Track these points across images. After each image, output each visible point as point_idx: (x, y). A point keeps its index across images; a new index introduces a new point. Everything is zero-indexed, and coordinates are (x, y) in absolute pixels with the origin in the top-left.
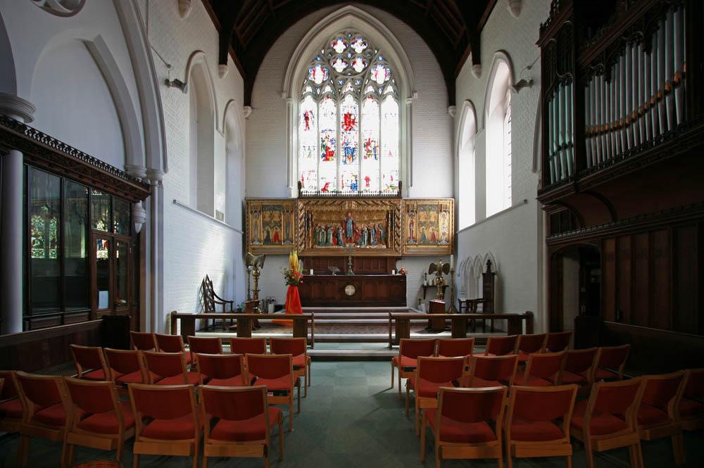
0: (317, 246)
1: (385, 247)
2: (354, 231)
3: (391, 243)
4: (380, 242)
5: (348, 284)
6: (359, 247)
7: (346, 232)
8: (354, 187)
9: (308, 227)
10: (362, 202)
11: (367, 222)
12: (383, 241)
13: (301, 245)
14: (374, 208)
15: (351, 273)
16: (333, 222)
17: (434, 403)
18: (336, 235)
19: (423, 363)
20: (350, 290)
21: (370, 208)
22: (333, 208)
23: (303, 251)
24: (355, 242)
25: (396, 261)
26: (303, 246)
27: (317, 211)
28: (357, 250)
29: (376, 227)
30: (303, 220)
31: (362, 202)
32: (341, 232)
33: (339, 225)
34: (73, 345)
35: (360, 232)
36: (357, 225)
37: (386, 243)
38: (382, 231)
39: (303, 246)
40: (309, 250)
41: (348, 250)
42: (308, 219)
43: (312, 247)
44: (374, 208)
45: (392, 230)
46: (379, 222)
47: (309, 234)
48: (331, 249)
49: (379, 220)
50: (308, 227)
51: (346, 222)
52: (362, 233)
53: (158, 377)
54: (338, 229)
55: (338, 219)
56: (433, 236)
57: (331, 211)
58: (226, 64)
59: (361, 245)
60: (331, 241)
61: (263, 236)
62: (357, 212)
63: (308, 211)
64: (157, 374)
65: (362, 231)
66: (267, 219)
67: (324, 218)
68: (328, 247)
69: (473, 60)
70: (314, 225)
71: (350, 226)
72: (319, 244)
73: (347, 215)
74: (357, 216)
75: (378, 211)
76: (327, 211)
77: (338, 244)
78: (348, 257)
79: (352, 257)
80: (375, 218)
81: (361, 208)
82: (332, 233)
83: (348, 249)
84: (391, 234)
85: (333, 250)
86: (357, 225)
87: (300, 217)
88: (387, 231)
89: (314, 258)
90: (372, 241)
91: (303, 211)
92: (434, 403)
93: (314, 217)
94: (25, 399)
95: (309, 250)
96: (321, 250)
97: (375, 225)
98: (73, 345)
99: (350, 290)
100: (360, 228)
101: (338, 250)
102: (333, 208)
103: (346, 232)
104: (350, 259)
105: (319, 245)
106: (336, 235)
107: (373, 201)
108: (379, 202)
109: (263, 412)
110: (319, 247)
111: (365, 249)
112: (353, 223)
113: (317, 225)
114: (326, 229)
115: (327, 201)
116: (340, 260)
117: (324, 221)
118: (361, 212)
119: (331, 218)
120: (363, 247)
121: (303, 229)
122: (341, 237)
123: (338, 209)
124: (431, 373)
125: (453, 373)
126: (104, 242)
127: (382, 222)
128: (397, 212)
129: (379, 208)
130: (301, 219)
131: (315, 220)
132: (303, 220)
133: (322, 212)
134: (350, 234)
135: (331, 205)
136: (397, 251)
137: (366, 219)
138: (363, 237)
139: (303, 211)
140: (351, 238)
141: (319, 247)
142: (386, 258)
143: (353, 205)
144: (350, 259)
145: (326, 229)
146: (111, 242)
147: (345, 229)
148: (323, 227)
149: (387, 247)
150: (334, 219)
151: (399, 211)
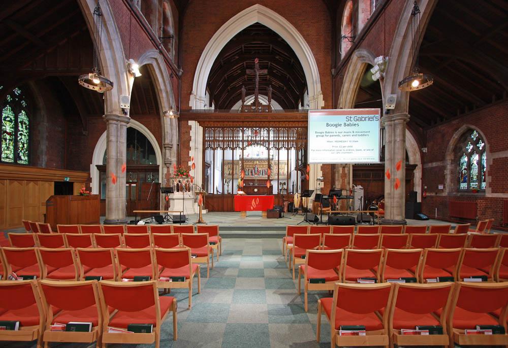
5: (254, 191)
8: (258, 155)
11: (262, 168)
15: (256, 185)
17: (304, 261)
18: (252, 172)
19: (297, 238)
20: (256, 190)
22: (251, 163)
32: (253, 171)
34: (134, 211)
48: (249, 177)
53: (88, 268)
56: (283, 173)
58: (332, 297)
61: (228, 173)
64: (87, 266)
66: (229, 167)
69: (301, 105)
71: (256, 169)
77: (252, 175)
83: (256, 177)
92: (304, 261)
96: (247, 177)
98: (134, 211)
99: (256, 190)
102: (251, 163)
106: (252, 172)
114: (248, 170)
116: (253, 181)
123: (252, 163)
124: (300, 242)
125: (314, 242)
126: (493, 219)
134: (256, 172)
145: (248, 170)
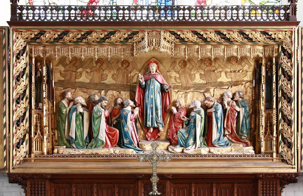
0: (63, 150)
1: (250, 150)
2: (166, 111)
3: (269, 140)
4: (236, 137)
6: (178, 149)
7: (143, 114)
9: (39, 99)
10: (189, 36)
11: (202, 88)
12: (245, 137)
13: (18, 146)
14: (220, 52)
16: (107, 88)
21: (208, 51)
22: (106, 52)
23: (25, 161)
24: (168, 139)
25: (282, 186)
26: (24, 148)
27: (62, 61)
28: (175, 158)
29: (226, 100)
30: (24, 81)
31: (189, 36)
33: (125, 95)
35: (183, 114)
36: (174, 97)
37: (254, 141)
38: (242, 111)
39: (24, 148)
40: (41, 158)
41: (149, 158)
42: (39, 81)
43: (51, 152)
44: (220, 52)
45: (269, 107)
46: (234, 89)
47: (40, 118)
49: (236, 84)
50: (39, 99)
51: (144, 89)
52: (188, 115)
54: (122, 105)
55: (120, 80)
57: (100, 61)
59: (186, 146)
60: (103, 136)
62: (173, 61)
63: (38, 59)
65: (189, 111)
67: (84, 79)
68: (95, 151)
70: (57, 93)
72: (70, 142)
73: (146, 70)
74: (174, 74)
75: (230, 59)
76: (91, 59)
77: (121, 144)
78: (150, 176)
79: (160, 175)
80: (223, 78)
81: (182, 52)
82: (105, 113)
84: (269, 118)
85: (108, 158)
86: (175, 96)
87: (15, 72)
88: (255, 112)
89: (55, 178)
90: (215, 135)
91: (24, 60)
93: (56, 77)
94: (18, 111)
95: (41, 158)
97: (222, 96)
100: (183, 103)
101: (123, 158)
102: (106, 52)
103: (143, 114)
104: (155, 180)
105: (69, 146)
107: (219, 33)
108: (235, 35)
109: (10, 182)
110: (72, 151)
111: (198, 157)
112: (163, 90)
113: (63, 96)
114: (90, 105)
115: (89, 33)
117: (83, 86)
118: (184, 63)
119: (102, 78)
120: (191, 150)
121: (24, 104)
122: (130, 127)
127: (241, 88)
128: (284, 60)
129: (234, 51)
130: (18, 79)
131: (60, 83)
132: (24, 81)
133: (77, 62)
135: (101, 42)
136: (283, 161)
137: (198, 80)
138: (190, 124)
139: (24, 60)
140: (157, 130)
141: (72, 151)
142: (254, 178)
143: (163, 43)
144: (155, 180)
145: (90, 105)
146: (80, 88)
147: (142, 106)
148: (81, 100)
149: (258, 151)
150: (109, 80)
151: (290, 56)
